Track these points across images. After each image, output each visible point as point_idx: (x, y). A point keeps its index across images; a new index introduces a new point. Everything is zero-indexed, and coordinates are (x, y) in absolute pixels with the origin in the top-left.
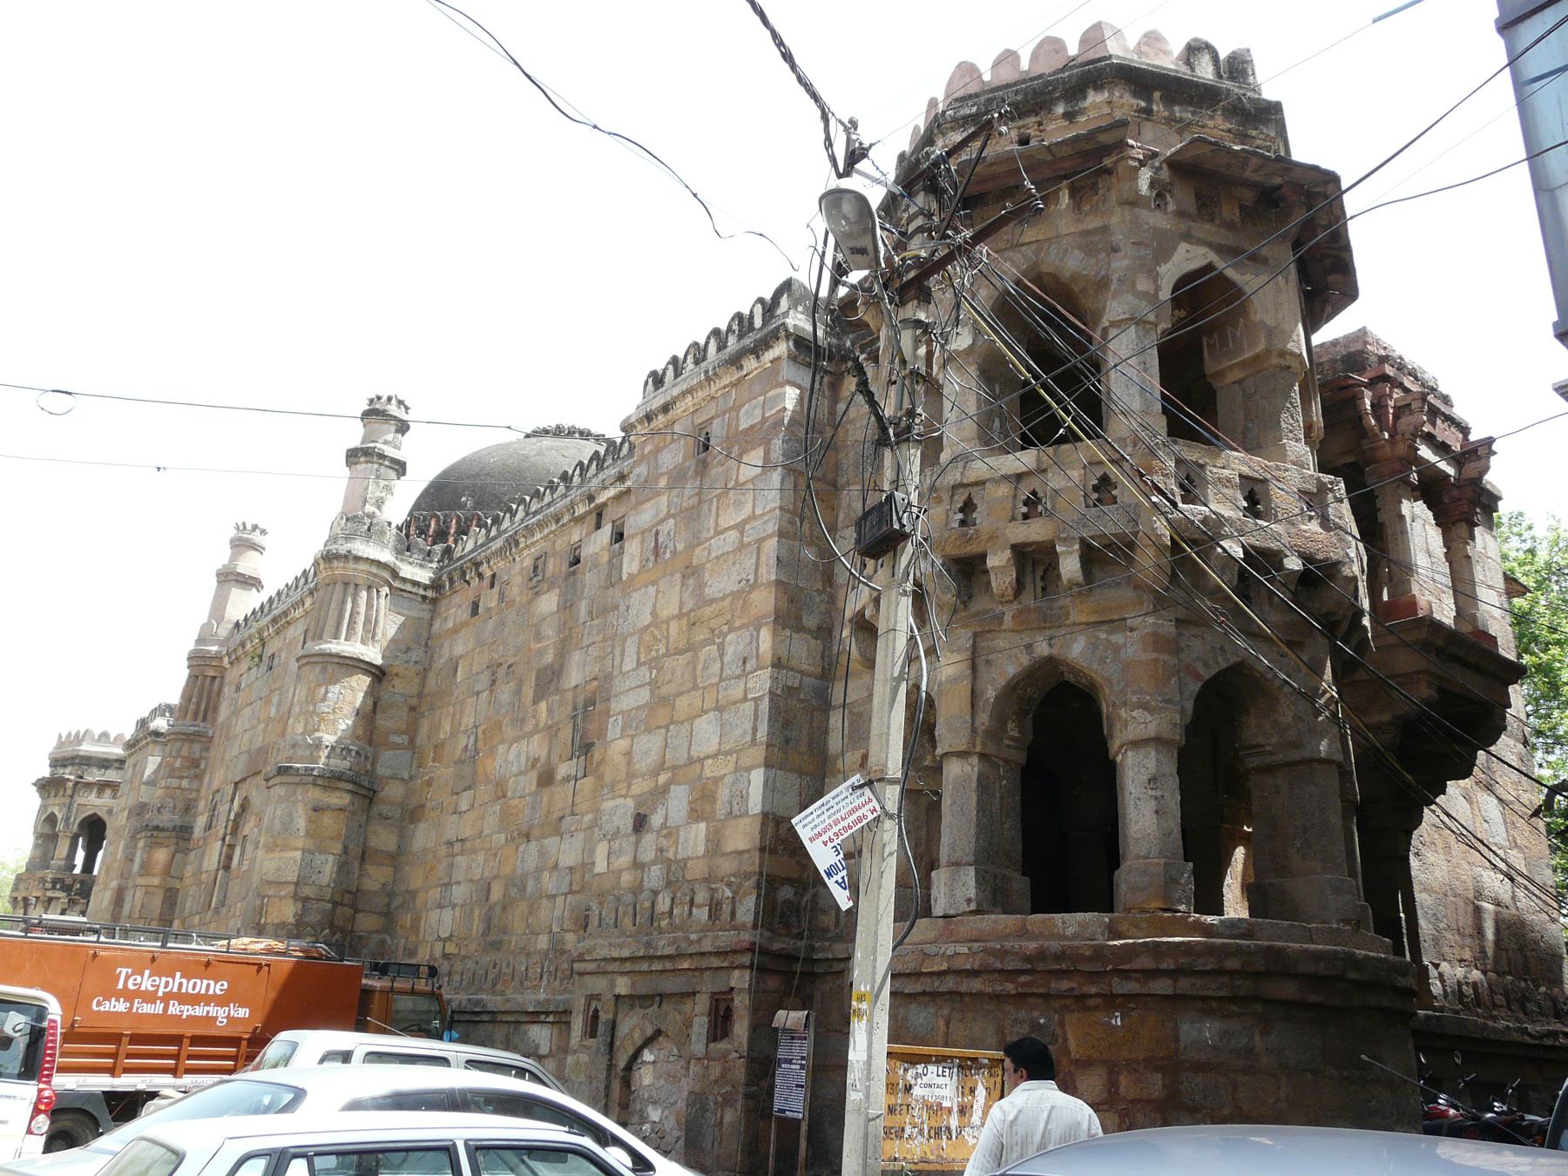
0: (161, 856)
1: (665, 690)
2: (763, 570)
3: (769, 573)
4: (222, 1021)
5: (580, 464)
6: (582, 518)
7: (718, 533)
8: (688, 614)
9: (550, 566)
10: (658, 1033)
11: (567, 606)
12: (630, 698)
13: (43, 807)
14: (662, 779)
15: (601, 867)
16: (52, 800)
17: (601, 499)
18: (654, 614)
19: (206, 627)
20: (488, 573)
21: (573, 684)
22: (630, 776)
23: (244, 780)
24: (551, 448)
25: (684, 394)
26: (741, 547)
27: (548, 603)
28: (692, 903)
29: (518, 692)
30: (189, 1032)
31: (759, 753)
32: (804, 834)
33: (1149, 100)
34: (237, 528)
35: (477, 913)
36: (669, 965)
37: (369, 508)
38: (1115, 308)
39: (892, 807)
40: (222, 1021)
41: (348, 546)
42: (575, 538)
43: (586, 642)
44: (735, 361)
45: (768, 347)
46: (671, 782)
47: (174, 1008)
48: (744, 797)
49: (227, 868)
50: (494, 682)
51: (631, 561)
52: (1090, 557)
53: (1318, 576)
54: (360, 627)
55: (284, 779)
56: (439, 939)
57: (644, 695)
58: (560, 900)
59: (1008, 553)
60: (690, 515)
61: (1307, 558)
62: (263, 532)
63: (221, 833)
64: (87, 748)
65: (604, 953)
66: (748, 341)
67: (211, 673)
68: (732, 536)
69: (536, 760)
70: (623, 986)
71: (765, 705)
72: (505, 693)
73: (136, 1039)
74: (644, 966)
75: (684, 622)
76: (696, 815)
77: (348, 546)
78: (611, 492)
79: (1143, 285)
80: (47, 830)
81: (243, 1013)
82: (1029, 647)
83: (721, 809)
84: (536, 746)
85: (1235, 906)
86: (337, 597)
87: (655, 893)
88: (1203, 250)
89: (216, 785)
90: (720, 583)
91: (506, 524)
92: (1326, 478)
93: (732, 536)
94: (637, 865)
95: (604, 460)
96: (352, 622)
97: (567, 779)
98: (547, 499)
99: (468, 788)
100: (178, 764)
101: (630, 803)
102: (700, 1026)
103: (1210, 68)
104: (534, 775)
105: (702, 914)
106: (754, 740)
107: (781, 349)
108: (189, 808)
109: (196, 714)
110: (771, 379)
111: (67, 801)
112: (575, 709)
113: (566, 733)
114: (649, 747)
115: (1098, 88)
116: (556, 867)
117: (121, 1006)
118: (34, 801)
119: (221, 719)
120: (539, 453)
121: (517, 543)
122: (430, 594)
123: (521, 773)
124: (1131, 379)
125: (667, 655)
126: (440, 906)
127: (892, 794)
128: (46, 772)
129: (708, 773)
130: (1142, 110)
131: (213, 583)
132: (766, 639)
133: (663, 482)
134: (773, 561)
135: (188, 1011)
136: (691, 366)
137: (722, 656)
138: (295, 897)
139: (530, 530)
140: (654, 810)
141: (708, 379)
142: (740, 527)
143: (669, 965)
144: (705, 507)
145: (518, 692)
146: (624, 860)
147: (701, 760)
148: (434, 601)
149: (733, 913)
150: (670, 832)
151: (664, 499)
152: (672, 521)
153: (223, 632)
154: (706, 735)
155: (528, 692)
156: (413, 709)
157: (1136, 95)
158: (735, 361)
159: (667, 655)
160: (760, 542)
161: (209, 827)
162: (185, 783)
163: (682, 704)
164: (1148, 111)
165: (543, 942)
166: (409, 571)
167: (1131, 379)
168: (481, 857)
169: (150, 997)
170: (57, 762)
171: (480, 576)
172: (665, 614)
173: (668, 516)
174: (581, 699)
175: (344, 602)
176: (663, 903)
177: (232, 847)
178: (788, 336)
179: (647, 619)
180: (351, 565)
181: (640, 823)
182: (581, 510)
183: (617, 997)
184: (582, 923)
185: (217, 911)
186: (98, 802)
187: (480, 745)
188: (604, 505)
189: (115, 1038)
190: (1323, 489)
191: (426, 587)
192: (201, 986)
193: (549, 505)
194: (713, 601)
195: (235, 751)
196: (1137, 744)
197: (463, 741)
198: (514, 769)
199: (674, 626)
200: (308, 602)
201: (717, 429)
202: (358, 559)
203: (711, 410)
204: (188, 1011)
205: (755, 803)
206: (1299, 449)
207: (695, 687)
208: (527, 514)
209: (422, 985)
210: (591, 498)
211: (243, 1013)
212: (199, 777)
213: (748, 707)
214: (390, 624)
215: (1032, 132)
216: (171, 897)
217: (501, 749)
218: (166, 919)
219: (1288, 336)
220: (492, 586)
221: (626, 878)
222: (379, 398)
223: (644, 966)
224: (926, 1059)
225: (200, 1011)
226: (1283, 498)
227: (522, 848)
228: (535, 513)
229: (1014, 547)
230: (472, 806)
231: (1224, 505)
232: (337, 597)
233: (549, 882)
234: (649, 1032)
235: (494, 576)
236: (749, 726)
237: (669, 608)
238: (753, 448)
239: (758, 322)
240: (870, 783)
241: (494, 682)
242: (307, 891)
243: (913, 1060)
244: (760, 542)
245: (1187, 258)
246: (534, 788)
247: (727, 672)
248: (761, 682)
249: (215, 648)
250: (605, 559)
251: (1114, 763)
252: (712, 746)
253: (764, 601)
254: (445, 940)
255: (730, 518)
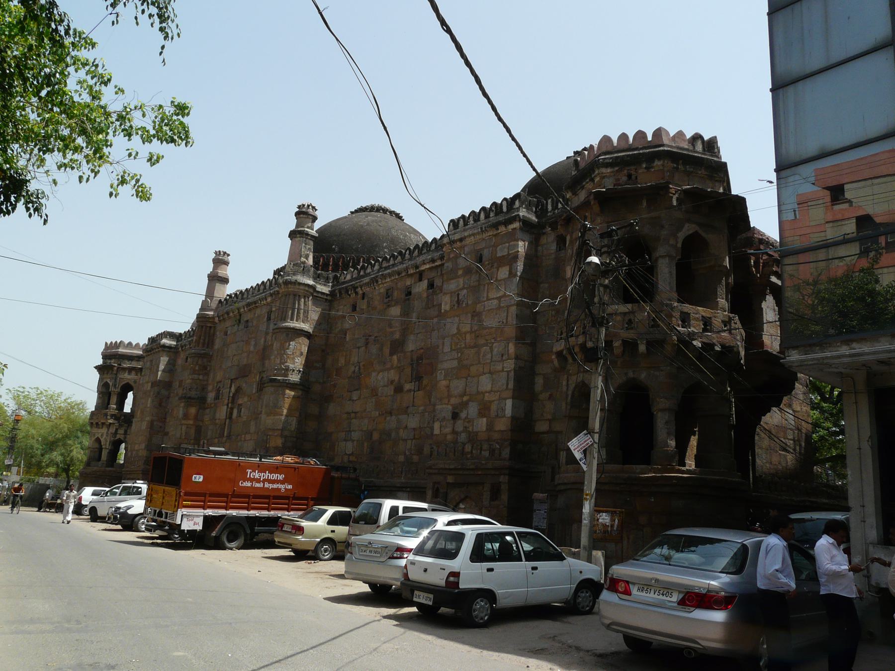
0: (193, 411)
1: (465, 362)
2: (510, 319)
3: (513, 320)
4: (283, 490)
5: (409, 249)
6: (412, 275)
7: (488, 299)
8: (475, 331)
9: (396, 294)
10: (466, 497)
11: (406, 313)
12: (448, 363)
13: (101, 380)
14: (465, 399)
15: (437, 431)
16: (105, 376)
17: (423, 268)
18: (458, 329)
19: (204, 303)
20: (361, 292)
21: (410, 349)
22: (449, 396)
23: (237, 379)
24: (373, 221)
25: (470, 236)
26: (499, 308)
27: (395, 311)
28: (481, 449)
29: (381, 349)
30: (272, 494)
31: (510, 393)
32: (572, 448)
33: (678, 164)
34: (216, 253)
35: (366, 444)
36: (472, 472)
37: (303, 259)
38: (661, 250)
39: (597, 441)
40: (283, 490)
41: (295, 278)
42: (408, 283)
43: (417, 332)
44: (496, 226)
45: (511, 223)
46: (469, 400)
47: (267, 485)
48: (503, 410)
49: (230, 418)
50: (367, 344)
51: (446, 304)
52: (649, 344)
53: (728, 351)
54: (302, 315)
55: (274, 384)
56: (346, 454)
57: (455, 363)
58: (409, 442)
59: (620, 342)
60: (475, 290)
61: (723, 346)
62: (228, 255)
63: (226, 401)
64: (121, 350)
65: (442, 466)
66: (501, 218)
67: (209, 325)
68: (495, 302)
69: (392, 382)
70: (450, 479)
71: (512, 374)
72: (374, 349)
73: (255, 497)
74: (461, 472)
75: (473, 335)
76: (481, 414)
77: (295, 278)
78: (428, 266)
79: (672, 242)
80: (104, 390)
81: (290, 487)
82: (626, 374)
83: (493, 413)
84: (393, 375)
85: (690, 463)
86: (291, 301)
87: (464, 444)
88: (694, 226)
89: (218, 378)
90: (491, 322)
91: (369, 270)
92: (732, 315)
93: (495, 302)
94: (454, 432)
95: (422, 250)
96: (298, 313)
97: (410, 391)
98: (392, 262)
99: (357, 390)
100: (197, 368)
101: (450, 407)
102: (486, 496)
103: (701, 147)
104: (392, 387)
105: (486, 454)
106: (507, 388)
107: (516, 225)
108: (204, 388)
109: (204, 344)
110: (512, 237)
111: (114, 376)
112: (412, 360)
113: (408, 371)
114: (458, 386)
115: (659, 160)
116: (406, 427)
117: (249, 484)
118: (96, 376)
119: (216, 347)
120: (368, 224)
121: (377, 282)
122: (329, 298)
123: (385, 386)
124: (665, 276)
125: (466, 347)
126: (345, 440)
127: (596, 436)
128: (100, 362)
129: (486, 398)
130: (674, 168)
131: (205, 281)
132: (512, 348)
133: (460, 272)
134: (514, 316)
135: (271, 486)
136: (472, 222)
137: (492, 351)
138: (282, 436)
139: (384, 277)
140: (462, 411)
141: (482, 231)
142: (499, 298)
143: (472, 472)
144: (482, 287)
145: (381, 349)
146: (448, 430)
147: (483, 393)
148: (330, 301)
149: (500, 453)
150: (469, 421)
151: (461, 281)
152: (465, 291)
153: (214, 305)
154: (485, 383)
155: (387, 350)
156: (323, 351)
157: (673, 162)
158: (496, 226)
159: (466, 347)
160: (508, 307)
161: (217, 398)
162: (201, 377)
163: (473, 369)
164: (677, 168)
165: (401, 458)
166: (320, 288)
167: (665, 276)
168: (366, 421)
169: (258, 481)
170: (105, 356)
171: (356, 293)
172: (464, 330)
173: (463, 288)
174: (415, 357)
175: (294, 304)
176: (468, 448)
177: (232, 409)
178: (520, 221)
179: (455, 331)
180: (297, 286)
181: (455, 416)
182: (411, 271)
183: (448, 483)
184: (420, 451)
185: (229, 436)
186: (129, 377)
187: (362, 370)
188: (423, 271)
189: (248, 496)
190: (730, 319)
191: (327, 295)
192: (275, 476)
193: (393, 265)
194: (486, 328)
195: (229, 364)
196: (663, 410)
197: (352, 368)
198: (382, 384)
199: (468, 336)
200: (269, 299)
201: (486, 253)
202: (300, 284)
203: (483, 245)
204: (271, 486)
205: (508, 412)
206: (723, 302)
207: (479, 363)
208: (381, 268)
209: (352, 476)
210: (417, 267)
211: (290, 487)
212: (207, 374)
213: (504, 374)
214: (314, 314)
215: (633, 172)
216: (198, 430)
217: (374, 374)
218: (197, 441)
219: (724, 260)
220: (363, 298)
221: (449, 437)
222: (304, 205)
223: (461, 472)
224: (603, 512)
225: (275, 486)
226: (717, 323)
227: (388, 418)
228: (386, 268)
229: (623, 340)
230: (359, 398)
231: (696, 327)
232: (291, 301)
233: (403, 434)
234: (463, 496)
235: (364, 294)
236: (504, 382)
237: (466, 328)
238: (504, 266)
239: (505, 209)
240: (589, 433)
241: (367, 344)
242: (286, 433)
243: (599, 512)
244: (508, 307)
245: (688, 229)
246: (392, 393)
247: (494, 359)
248: (510, 365)
249: (212, 313)
250: (425, 295)
251: (653, 414)
252: (489, 388)
253: (511, 331)
254: (349, 455)
255: (493, 294)
